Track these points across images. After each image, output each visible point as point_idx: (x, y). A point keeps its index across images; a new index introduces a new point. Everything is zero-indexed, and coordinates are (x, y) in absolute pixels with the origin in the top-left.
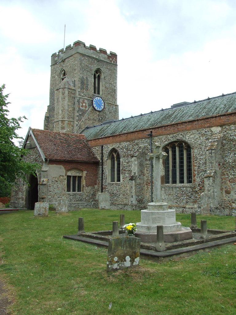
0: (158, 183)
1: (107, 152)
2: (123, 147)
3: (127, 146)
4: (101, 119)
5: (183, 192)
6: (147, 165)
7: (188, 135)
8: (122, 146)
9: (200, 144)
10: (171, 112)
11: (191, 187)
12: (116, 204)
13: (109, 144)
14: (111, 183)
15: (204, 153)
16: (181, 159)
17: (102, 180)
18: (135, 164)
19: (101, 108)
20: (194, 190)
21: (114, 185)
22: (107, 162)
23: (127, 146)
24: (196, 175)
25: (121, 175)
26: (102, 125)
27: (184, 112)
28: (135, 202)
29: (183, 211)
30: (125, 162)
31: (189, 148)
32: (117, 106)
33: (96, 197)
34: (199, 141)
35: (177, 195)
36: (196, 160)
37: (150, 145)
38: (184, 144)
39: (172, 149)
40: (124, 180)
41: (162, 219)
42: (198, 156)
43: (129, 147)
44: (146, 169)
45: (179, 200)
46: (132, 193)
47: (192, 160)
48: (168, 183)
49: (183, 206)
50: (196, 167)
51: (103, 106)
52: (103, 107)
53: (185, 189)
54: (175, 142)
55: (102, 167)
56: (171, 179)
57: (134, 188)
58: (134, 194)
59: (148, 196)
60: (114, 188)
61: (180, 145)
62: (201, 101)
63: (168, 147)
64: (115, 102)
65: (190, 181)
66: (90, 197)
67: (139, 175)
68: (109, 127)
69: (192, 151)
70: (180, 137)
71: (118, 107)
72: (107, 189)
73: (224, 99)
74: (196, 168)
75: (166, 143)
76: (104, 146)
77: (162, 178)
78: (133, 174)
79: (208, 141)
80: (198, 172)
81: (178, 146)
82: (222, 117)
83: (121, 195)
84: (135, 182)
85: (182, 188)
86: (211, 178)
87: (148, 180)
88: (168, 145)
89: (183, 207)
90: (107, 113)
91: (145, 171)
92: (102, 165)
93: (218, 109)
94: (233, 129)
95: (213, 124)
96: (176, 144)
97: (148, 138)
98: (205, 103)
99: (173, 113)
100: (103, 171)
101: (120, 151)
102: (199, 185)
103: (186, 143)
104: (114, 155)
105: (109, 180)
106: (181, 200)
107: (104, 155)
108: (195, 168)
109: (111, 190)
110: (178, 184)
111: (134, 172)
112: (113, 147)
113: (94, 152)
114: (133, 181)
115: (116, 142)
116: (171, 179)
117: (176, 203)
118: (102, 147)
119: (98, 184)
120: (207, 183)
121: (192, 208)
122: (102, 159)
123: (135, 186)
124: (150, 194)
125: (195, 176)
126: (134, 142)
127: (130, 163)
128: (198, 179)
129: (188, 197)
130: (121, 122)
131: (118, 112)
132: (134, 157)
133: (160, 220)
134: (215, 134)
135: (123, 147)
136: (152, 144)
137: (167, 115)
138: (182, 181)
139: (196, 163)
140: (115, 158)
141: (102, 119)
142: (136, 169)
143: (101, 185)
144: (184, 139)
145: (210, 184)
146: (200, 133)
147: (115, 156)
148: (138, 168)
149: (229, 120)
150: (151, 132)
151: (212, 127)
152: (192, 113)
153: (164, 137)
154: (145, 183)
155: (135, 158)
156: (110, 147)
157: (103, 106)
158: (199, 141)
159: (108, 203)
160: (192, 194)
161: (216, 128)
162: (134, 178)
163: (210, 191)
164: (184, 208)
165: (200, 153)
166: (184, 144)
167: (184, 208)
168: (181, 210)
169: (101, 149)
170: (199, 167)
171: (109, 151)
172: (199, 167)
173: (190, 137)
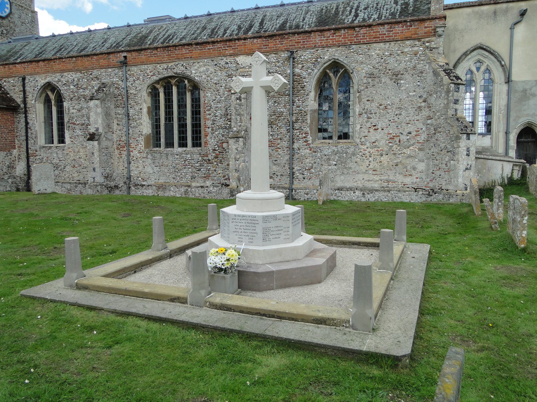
0: (139, 146)
1: (34, 90)
2: (68, 81)
3: (76, 79)
4: (5, 32)
5: (185, 161)
6: (118, 116)
7: (196, 68)
8: (66, 80)
9: (216, 84)
10: (145, 31)
11: (200, 154)
12: (58, 182)
13: (38, 73)
14: (47, 145)
15: (223, 99)
16: (182, 106)
17: (27, 140)
18: (97, 114)
19: (5, 12)
20: (205, 158)
21: (53, 149)
22: (35, 108)
23: (76, 79)
24: (208, 134)
25: (66, 131)
26: (10, 42)
27: (170, 32)
28: (100, 179)
29: (186, 192)
30: (73, 109)
31: (195, 87)
32: (34, 13)
33: (15, 171)
34: (216, 78)
35: (174, 165)
36: (209, 110)
37: (122, 81)
38: (186, 82)
39: (165, 89)
40: (72, 141)
41: (284, 230)
42: (212, 103)
43: (80, 83)
44: (116, 122)
45: (179, 174)
46: (93, 163)
47: (202, 110)
48: (185, 145)
49: (187, 184)
50: (209, 122)
51: (7, 8)
52: (8, 11)
53: (189, 156)
54: (171, 77)
55: (26, 117)
56: (163, 140)
57: (96, 154)
58: (97, 166)
59: (121, 168)
60: (56, 153)
61: (179, 83)
62: (196, 17)
63: (158, 86)
64: (30, 5)
65: (197, 143)
66: (4, 171)
67: (105, 133)
68: (27, 48)
69: (202, 94)
70: (179, 69)
71: (37, 14)
72: (38, 157)
73: (235, 17)
74: (209, 123)
75: (155, 78)
76: (28, 77)
77: (147, 138)
78: (92, 130)
79: (230, 79)
80: (212, 130)
81: (175, 85)
82: (255, 40)
83: (68, 167)
84: (99, 144)
85: (183, 155)
86: (241, 139)
87: (120, 141)
88: (158, 82)
89: (185, 186)
90: (16, 22)
91: (115, 127)
92: (26, 112)
93: (228, 31)
94: (274, 61)
95: (239, 51)
96: (173, 81)
97: (120, 67)
98: (204, 21)
99: (151, 32)
100: (27, 123)
101: (63, 90)
102: (215, 150)
103: (190, 80)
104: (53, 97)
105: (41, 140)
106: (183, 174)
107: (27, 94)
108: (206, 122)
109: (47, 158)
110: (177, 149)
111: (96, 126)
112: (47, 81)
113: (5, 87)
114: (96, 143)
115: (55, 72)
116: (163, 140)
117: (174, 178)
118: (24, 79)
119: (19, 147)
120: (234, 147)
121: (202, 187)
122: (25, 102)
123: (100, 151)
124: (126, 166)
125: (207, 136)
126: (91, 74)
127: (84, 111)
128: (213, 141)
129: (194, 170)
130: (50, 40)
131: (38, 25)
132: (94, 101)
133: (279, 232)
134: (243, 68)
135: (68, 81)
136: (127, 79)
137: (139, 34)
138: (183, 144)
139: (210, 115)
140: (53, 102)
141: (8, 33)
142: (100, 121)
143: (24, 149)
144: (188, 73)
145: (239, 149)
146: (216, 65)
147: (52, 97)
148: (103, 120)
149: (268, 45)
150: (125, 57)
151: (237, 55)
152: (183, 34)
153: (151, 67)
154: (115, 146)
155: (97, 102)
156: (42, 81)
157: (7, 8)
158: (216, 78)
159: (52, 183)
160: (201, 165)
161: (245, 58)
162: (97, 137)
163: (238, 160)
164: (189, 186)
165: (216, 97)
166: (186, 82)
167: (189, 186)
168: (183, 190)
169: (20, 83)
170: (214, 121)
171: (39, 88)
172: (214, 121)
173: (199, 70)
